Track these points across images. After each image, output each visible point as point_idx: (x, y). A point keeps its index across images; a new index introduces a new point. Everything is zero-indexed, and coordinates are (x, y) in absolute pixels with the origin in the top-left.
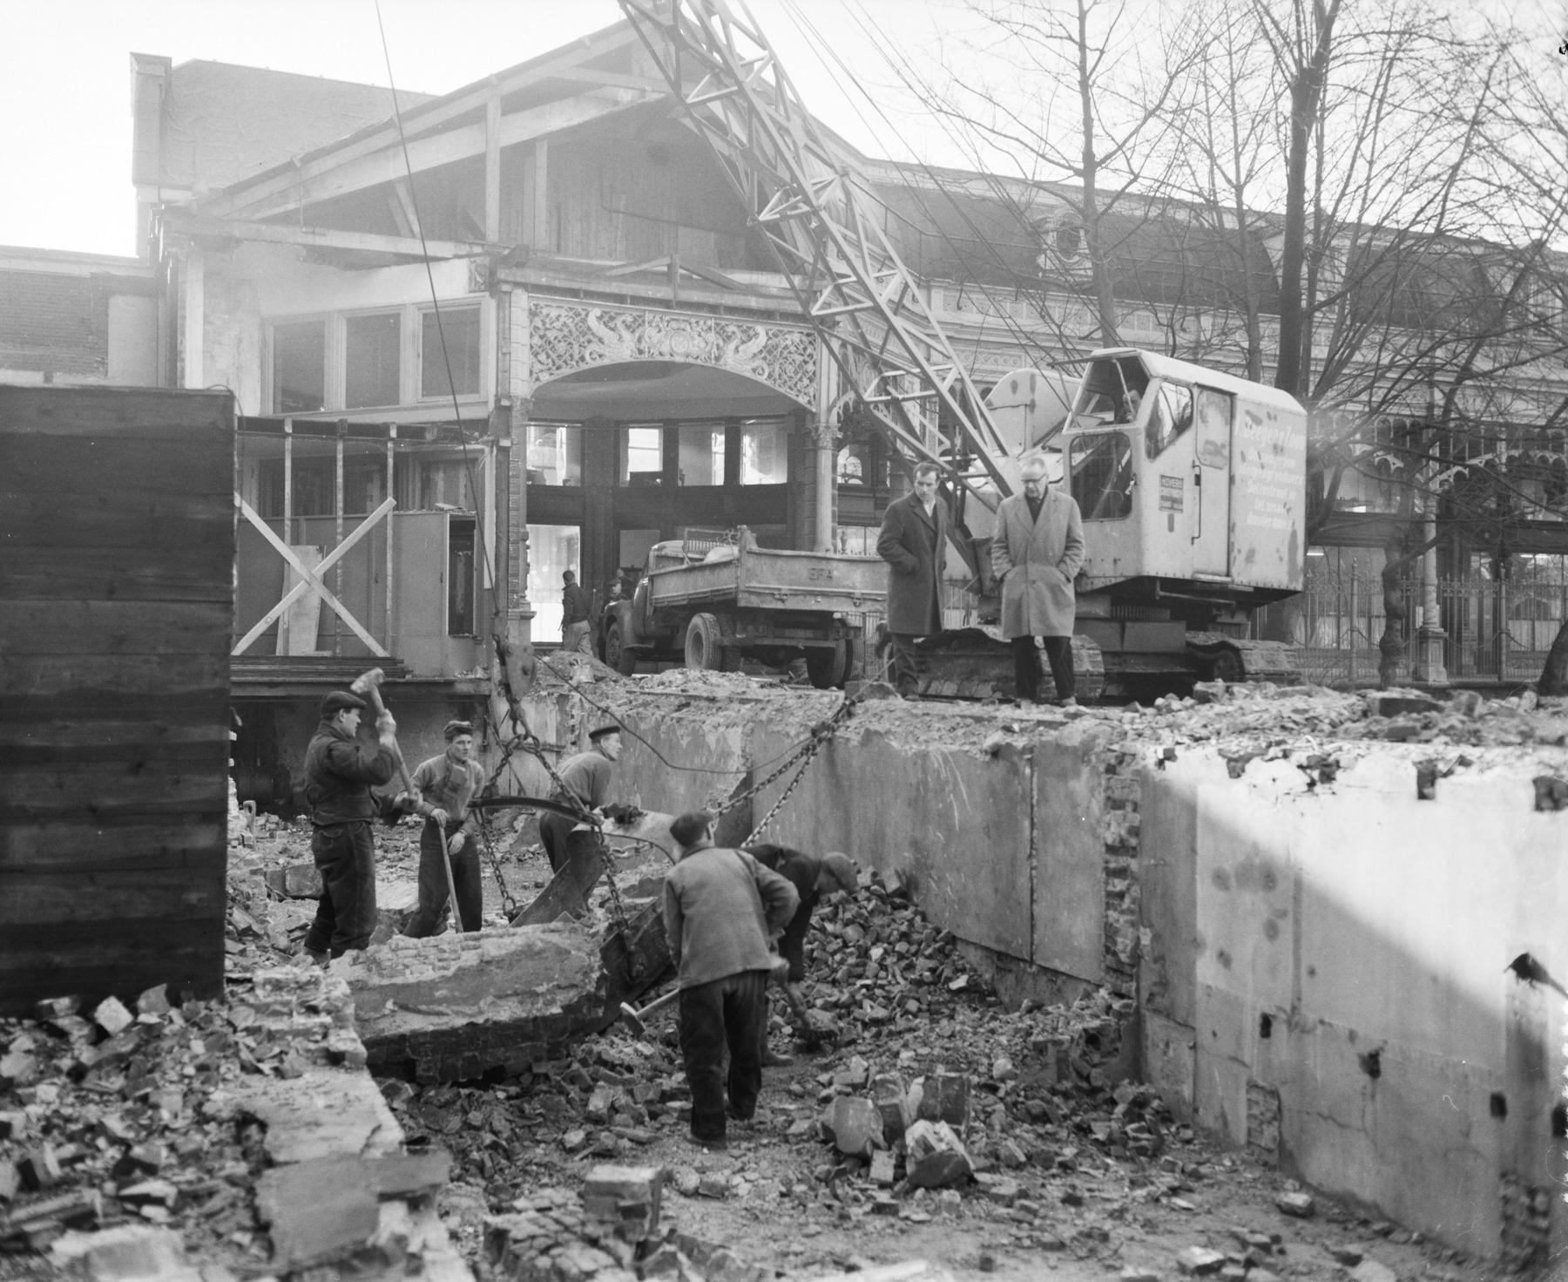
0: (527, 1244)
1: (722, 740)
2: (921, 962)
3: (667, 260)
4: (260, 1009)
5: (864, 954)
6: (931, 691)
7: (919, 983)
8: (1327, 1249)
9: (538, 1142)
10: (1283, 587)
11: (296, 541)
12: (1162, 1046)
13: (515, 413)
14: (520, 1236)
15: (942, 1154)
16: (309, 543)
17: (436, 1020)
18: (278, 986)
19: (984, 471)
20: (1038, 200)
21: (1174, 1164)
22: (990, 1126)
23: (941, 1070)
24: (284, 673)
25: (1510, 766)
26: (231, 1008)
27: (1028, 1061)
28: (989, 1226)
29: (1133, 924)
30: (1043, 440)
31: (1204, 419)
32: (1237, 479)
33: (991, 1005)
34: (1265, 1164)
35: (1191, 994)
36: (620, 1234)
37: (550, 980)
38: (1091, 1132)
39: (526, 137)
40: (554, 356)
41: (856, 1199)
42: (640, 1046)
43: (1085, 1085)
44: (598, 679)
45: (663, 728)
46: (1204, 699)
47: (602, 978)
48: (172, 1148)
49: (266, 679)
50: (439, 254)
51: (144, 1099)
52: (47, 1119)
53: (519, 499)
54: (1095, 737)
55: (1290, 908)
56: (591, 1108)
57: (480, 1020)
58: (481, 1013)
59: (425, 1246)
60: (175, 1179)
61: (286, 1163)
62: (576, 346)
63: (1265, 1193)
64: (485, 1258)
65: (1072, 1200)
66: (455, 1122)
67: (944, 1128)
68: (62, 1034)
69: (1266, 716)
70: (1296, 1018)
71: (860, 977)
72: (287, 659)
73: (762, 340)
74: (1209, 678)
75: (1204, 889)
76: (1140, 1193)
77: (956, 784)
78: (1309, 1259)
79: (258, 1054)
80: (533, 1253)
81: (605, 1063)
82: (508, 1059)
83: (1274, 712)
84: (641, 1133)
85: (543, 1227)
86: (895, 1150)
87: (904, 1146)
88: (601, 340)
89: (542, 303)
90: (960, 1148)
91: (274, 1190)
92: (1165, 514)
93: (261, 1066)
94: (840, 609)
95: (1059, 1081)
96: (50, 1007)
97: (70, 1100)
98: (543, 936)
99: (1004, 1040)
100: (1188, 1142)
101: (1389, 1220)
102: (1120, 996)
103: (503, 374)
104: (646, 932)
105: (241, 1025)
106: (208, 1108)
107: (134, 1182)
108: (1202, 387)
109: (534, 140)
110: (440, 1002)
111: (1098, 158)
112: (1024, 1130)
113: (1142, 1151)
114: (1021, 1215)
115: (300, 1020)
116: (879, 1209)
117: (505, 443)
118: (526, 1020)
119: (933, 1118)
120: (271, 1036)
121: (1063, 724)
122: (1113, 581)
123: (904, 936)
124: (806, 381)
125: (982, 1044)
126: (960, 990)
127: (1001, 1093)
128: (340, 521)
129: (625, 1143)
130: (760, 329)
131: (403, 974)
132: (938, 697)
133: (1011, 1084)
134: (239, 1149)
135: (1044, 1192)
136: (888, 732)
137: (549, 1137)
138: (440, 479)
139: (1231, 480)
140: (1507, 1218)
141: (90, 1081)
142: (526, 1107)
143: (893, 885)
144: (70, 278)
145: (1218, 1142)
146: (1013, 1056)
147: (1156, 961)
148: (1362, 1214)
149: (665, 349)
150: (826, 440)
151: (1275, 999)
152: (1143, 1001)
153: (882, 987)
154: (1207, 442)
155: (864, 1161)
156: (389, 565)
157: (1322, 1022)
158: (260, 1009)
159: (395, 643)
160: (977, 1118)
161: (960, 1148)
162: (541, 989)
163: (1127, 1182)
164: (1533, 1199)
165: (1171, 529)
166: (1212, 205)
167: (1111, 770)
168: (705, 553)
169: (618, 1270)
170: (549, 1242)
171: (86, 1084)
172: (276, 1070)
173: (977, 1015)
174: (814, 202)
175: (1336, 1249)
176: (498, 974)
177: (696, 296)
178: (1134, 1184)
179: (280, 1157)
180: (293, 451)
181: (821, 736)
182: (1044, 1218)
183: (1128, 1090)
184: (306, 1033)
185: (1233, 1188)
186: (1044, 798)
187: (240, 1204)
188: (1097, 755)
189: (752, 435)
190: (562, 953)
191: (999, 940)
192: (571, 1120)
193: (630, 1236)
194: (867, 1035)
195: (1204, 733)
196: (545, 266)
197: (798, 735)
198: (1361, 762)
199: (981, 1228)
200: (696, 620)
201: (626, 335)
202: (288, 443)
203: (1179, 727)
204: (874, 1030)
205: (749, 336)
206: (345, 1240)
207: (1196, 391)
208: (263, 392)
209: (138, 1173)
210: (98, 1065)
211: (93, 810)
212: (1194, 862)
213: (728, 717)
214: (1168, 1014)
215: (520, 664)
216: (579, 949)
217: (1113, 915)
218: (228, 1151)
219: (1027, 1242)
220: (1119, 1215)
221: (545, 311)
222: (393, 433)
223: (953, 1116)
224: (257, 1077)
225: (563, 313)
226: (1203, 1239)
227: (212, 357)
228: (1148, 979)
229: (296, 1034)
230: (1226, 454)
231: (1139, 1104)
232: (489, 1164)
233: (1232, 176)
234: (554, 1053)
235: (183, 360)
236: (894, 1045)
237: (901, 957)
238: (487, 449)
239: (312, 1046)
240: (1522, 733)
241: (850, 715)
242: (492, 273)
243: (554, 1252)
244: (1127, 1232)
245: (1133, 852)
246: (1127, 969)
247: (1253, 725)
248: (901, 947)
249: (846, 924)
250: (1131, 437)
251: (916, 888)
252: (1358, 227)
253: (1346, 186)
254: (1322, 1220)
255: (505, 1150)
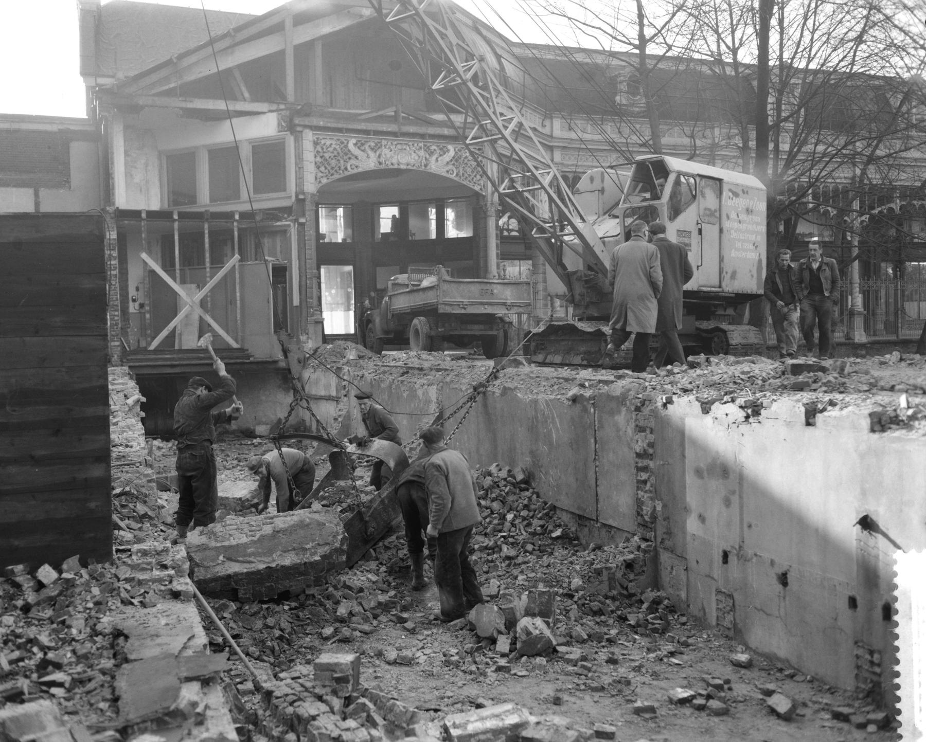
0: (282, 699)
1: (426, 393)
2: (536, 522)
3: (394, 109)
4: (133, 567)
5: (503, 518)
6: (547, 361)
7: (534, 534)
8: (756, 686)
9: (308, 634)
10: (754, 292)
11: (183, 282)
12: (669, 568)
13: (307, 202)
14: (279, 695)
15: (536, 636)
16: (191, 282)
17: (247, 565)
18: (145, 553)
19: (572, 231)
20: (613, 63)
21: (674, 638)
22: (569, 618)
23: (541, 587)
24: (180, 359)
25: (858, 405)
26: (117, 567)
27: (592, 579)
28: (561, 677)
29: (652, 499)
30: (609, 212)
31: (703, 196)
33: (575, 546)
34: (727, 637)
35: (685, 538)
36: (335, 693)
37: (313, 541)
38: (627, 620)
39: (308, 39)
40: (329, 168)
41: (487, 664)
42: (370, 576)
43: (625, 592)
44: (360, 357)
45: (394, 386)
46: (693, 366)
47: (344, 539)
48: (74, 652)
49: (168, 363)
50: (260, 110)
51: (63, 622)
52: (7, 635)
53: (312, 253)
54: (629, 390)
55: (737, 490)
56: (338, 614)
57: (273, 565)
58: (274, 561)
59: (207, 707)
60: (71, 671)
61: (135, 660)
62: (342, 162)
63: (725, 653)
64: (261, 707)
65: (612, 661)
66: (259, 624)
67: (539, 621)
68: (18, 586)
69: (725, 376)
70: (742, 553)
71: (500, 531)
72: (181, 351)
73: (452, 153)
74: (697, 353)
75: (690, 478)
76: (652, 655)
77: (553, 418)
78: (746, 693)
79: (131, 594)
80: (286, 704)
81: (350, 588)
82: (291, 586)
83: (730, 373)
84: (366, 627)
85: (293, 689)
86: (512, 634)
87: (515, 632)
88: (356, 158)
89: (321, 137)
90: (547, 633)
91: (125, 677)
93: (133, 600)
94: (500, 312)
95: (610, 591)
96: (12, 570)
97: (22, 624)
98: (310, 516)
99: (578, 567)
100: (684, 624)
101: (795, 669)
102: (646, 540)
103: (300, 179)
104: (375, 509)
105: (122, 577)
106: (99, 627)
107: (48, 674)
108: (702, 176)
109: (313, 40)
110: (250, 555)
111: (647, 37)
112: (589, 621)
113: (655, 631)
114: (580, 671)
115: (157, 573)
116: (499, 669)
117: (302, 220)
118: (300, 564)
119: (533, 615)
120: (140, 583)
121: (612, 382)
123: (526, 507)
124: (478, 177)
125: (565, 570)
126: (558, 538)
127: (576, 599)
128: (208, 270)
129: (358, 634)
130: (450, 147)
131: (229, 540)
132: (551, 364)
133: (581, 593)
134: (112, 651)
135: (596, 656)
136: (516, 388)
137: (314, 631)
138: (267, 242)
139: (721, 231)
140: (858, 667)
141: (33, 613)
142: (301, 614)
143: (520, 477)
144: (46, 132)
145: (700, 623)
146: (583, 577)
147: (664, 520)
148: (779, 665)
149: (394, 161)
150: (492, 211)
151: (730, 542)
152: (658, 543)
153: (513, 537)
154: (706, 209)
155: (493, 641)
156: (238, 294)
157: (756, 555)
158: (133, 567)
159: (243, 340)
160: (561, 614)
161: (547, 633)
162: (308, 546)
163: (645, 650)
164: (872, 657)
166: (719, 61)
167: (638, 409)
168: (421, 281)
169: (331, 714)
170: (295, 698)
171: (30, 615)
172: (141, 602)
173: (566, 552)
174: (464, 77)
175: (761, 686)
176: (283, 539)
177: (412, 129)
178: (649, 650)
179: (132, 657)
180: (179, 230)
181: (479, 390)
182: (595, 672)
183: (650, 595)
184: (160, 581)
185: (706, 651)
186: (602, 426)
187: (106, 685)
188: (630, 400)
189: (452, 208)
190: (321, 525)
191: (579, 508)
192: (327, 621)
193: (340, 694)
194: (503, 565)
195: (690, 387)
196: (322, 115)
197: (467, 390)
198: (774, 404)
199: (557, 679)
200: (415, 321)
201: (372, 154)
202: (176, 225)
203: (676, 383)
204: (507, 562)
205: (444, 151)
206: (158, 707)
207: (698, 179)
208: (161, 195)
209: (50, 668)
210: (38, 604)
211: (32, 457)
212: (684, 463)
213: (429, 380)
214: (672, 551)
215: (296, 357)
216: (331, 522)
217: (641, 493)
218: (105, 653)
219: (583, 687)
220: (638, 669)
221: (323, 142)
222: (237, 217)
223: (545, 613)
224: (131, 606)
225: (334, 142)
226: (685, 682)
227: (131, 176)
228: (661, 530)
229: (154, 581)
230: (716, 216)
231: (656, 602)
232: (277, 648)
233: (730, 45)
234: (318, 582)
235: (113, 178)
236: (515, 572)
237: (524, 519)
238: (292, 224)
239: (163, 588)
240: (871, 384)
241: (496, 378)
242: (291, 120)
243: (296, 704)
244: (643, 679)
245: (651, 457)
246: (649, 525)
247: (718, 381)
248: (524, 513)
249: (493, 501)
250: (659, 209)
251: (534, 479)
252: (806, 71)
253: (798, 47)
254: (756, 669)
255: (287, 640)
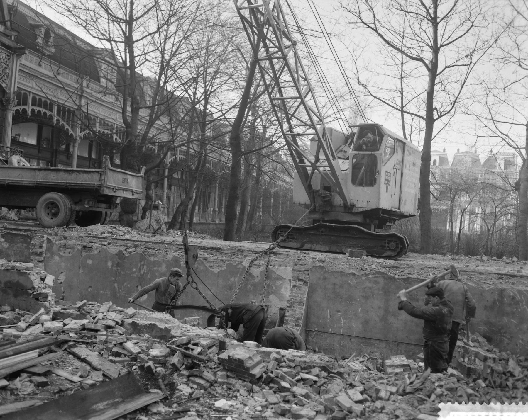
32: (404, 174)
92: (386, 186)
122: (367, 209)
124: (6, 77)
165: (387, 192)
